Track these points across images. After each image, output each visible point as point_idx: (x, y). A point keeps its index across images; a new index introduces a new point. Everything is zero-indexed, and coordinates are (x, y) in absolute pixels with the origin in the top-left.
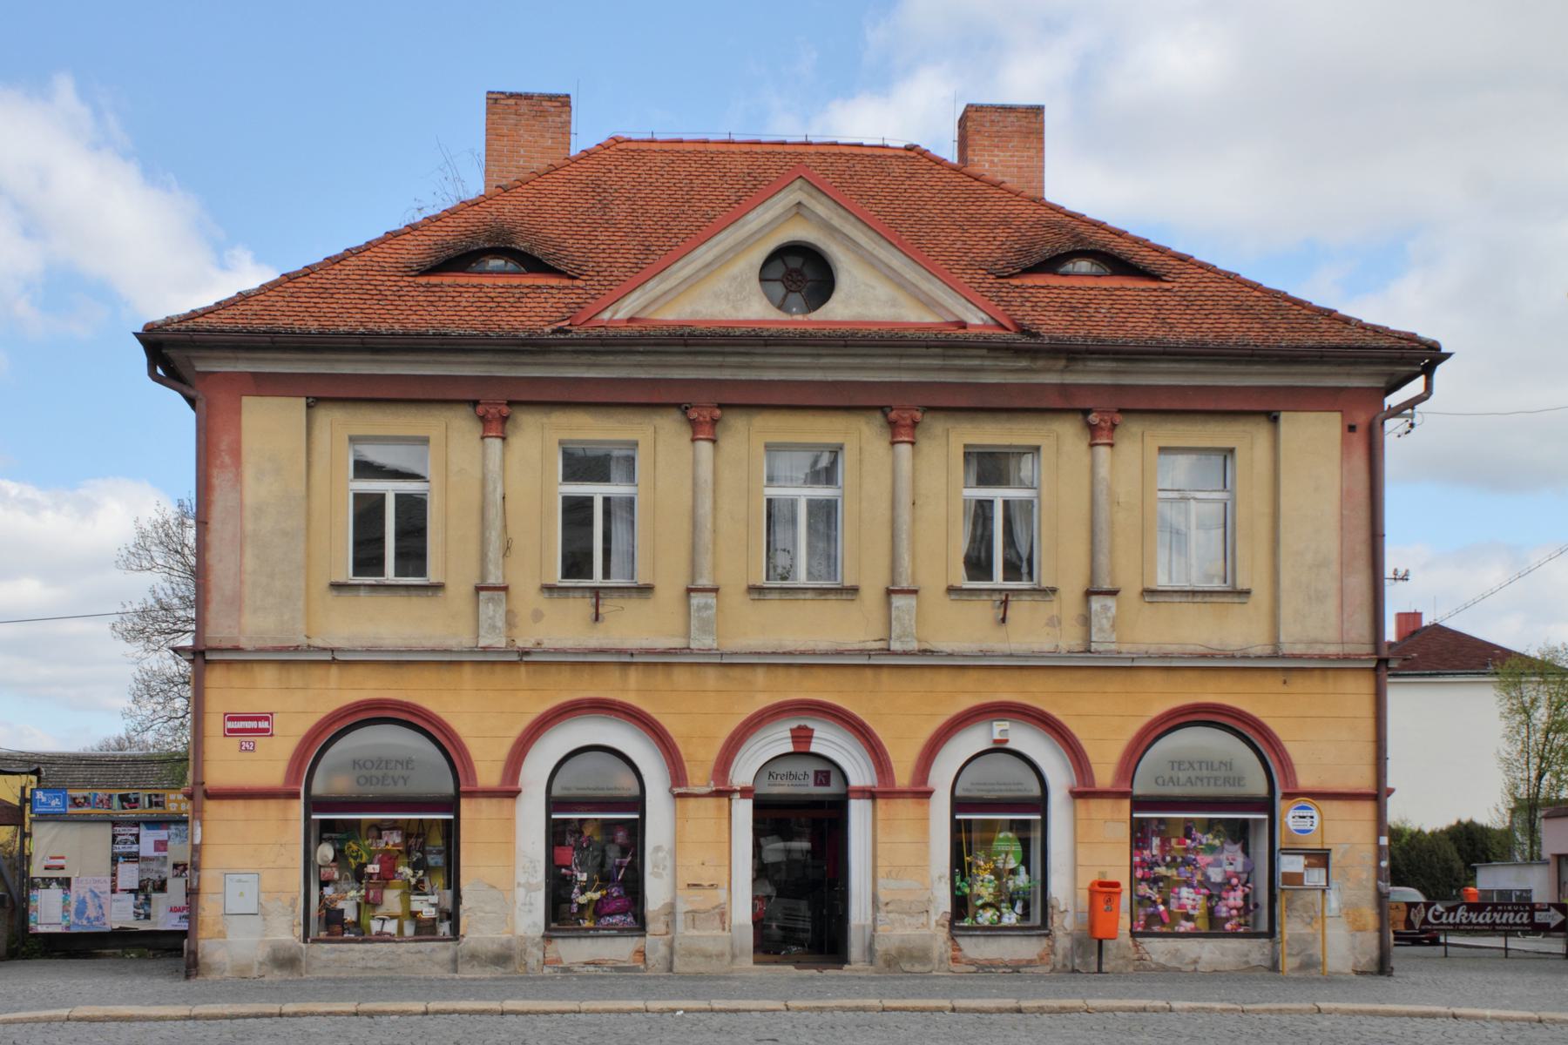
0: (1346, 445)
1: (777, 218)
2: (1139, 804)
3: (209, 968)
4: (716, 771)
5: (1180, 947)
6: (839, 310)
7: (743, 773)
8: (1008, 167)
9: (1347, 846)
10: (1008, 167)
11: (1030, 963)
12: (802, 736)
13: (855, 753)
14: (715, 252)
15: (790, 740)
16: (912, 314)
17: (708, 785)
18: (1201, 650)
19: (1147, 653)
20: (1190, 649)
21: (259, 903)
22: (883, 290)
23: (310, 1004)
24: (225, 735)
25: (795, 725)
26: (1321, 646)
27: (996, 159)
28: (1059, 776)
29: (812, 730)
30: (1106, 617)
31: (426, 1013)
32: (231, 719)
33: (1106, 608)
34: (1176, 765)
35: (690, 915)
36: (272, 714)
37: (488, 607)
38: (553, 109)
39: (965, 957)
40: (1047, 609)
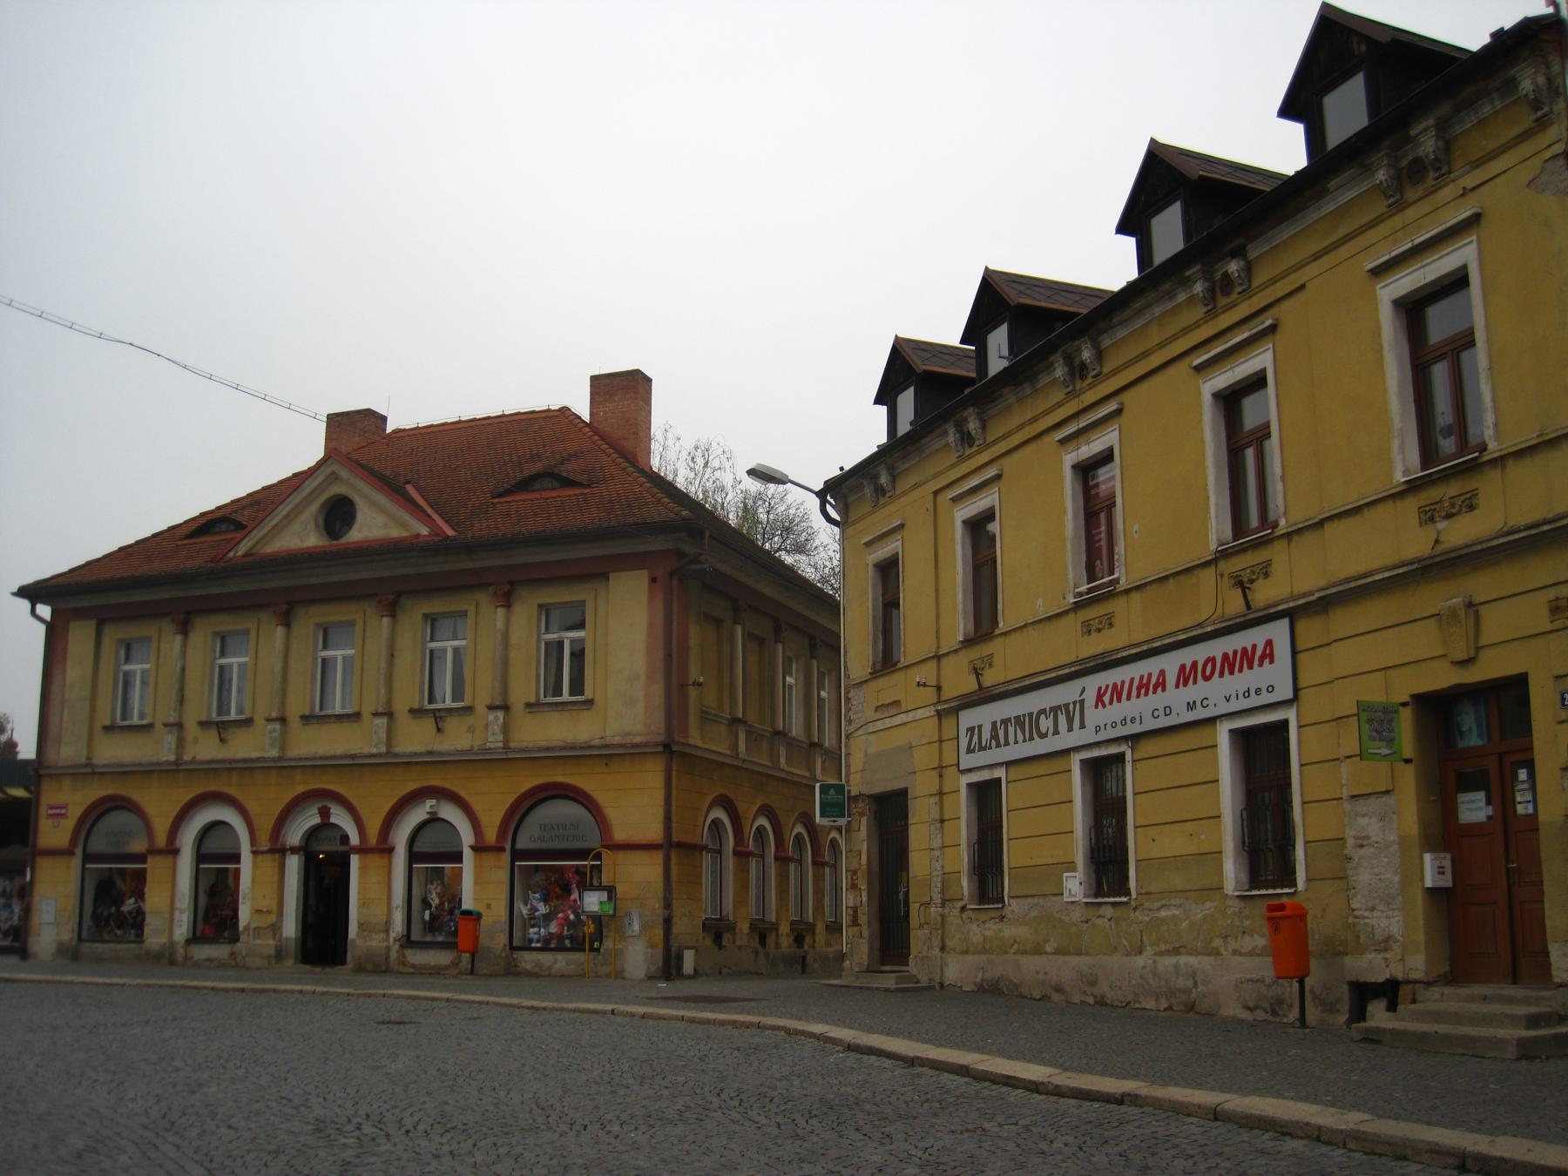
1: (321, 484)
4: (271, 837)
5: (540, 957)
7: (294, 836)
9: (645, 884)
11: (447, 967)
12: (325, 813)
14: (289, 508)
16: (396, 533)
18: (560, 744)
20: (554, 744)
22: (380, 519)
25: (320, 805)
26: (631, 737)
27: (607, 410)
28: (467, 837)
29: (330, 808)
30: (498, 725)
32: (51, 808)
33: (497, 718)
34: (543, 827)
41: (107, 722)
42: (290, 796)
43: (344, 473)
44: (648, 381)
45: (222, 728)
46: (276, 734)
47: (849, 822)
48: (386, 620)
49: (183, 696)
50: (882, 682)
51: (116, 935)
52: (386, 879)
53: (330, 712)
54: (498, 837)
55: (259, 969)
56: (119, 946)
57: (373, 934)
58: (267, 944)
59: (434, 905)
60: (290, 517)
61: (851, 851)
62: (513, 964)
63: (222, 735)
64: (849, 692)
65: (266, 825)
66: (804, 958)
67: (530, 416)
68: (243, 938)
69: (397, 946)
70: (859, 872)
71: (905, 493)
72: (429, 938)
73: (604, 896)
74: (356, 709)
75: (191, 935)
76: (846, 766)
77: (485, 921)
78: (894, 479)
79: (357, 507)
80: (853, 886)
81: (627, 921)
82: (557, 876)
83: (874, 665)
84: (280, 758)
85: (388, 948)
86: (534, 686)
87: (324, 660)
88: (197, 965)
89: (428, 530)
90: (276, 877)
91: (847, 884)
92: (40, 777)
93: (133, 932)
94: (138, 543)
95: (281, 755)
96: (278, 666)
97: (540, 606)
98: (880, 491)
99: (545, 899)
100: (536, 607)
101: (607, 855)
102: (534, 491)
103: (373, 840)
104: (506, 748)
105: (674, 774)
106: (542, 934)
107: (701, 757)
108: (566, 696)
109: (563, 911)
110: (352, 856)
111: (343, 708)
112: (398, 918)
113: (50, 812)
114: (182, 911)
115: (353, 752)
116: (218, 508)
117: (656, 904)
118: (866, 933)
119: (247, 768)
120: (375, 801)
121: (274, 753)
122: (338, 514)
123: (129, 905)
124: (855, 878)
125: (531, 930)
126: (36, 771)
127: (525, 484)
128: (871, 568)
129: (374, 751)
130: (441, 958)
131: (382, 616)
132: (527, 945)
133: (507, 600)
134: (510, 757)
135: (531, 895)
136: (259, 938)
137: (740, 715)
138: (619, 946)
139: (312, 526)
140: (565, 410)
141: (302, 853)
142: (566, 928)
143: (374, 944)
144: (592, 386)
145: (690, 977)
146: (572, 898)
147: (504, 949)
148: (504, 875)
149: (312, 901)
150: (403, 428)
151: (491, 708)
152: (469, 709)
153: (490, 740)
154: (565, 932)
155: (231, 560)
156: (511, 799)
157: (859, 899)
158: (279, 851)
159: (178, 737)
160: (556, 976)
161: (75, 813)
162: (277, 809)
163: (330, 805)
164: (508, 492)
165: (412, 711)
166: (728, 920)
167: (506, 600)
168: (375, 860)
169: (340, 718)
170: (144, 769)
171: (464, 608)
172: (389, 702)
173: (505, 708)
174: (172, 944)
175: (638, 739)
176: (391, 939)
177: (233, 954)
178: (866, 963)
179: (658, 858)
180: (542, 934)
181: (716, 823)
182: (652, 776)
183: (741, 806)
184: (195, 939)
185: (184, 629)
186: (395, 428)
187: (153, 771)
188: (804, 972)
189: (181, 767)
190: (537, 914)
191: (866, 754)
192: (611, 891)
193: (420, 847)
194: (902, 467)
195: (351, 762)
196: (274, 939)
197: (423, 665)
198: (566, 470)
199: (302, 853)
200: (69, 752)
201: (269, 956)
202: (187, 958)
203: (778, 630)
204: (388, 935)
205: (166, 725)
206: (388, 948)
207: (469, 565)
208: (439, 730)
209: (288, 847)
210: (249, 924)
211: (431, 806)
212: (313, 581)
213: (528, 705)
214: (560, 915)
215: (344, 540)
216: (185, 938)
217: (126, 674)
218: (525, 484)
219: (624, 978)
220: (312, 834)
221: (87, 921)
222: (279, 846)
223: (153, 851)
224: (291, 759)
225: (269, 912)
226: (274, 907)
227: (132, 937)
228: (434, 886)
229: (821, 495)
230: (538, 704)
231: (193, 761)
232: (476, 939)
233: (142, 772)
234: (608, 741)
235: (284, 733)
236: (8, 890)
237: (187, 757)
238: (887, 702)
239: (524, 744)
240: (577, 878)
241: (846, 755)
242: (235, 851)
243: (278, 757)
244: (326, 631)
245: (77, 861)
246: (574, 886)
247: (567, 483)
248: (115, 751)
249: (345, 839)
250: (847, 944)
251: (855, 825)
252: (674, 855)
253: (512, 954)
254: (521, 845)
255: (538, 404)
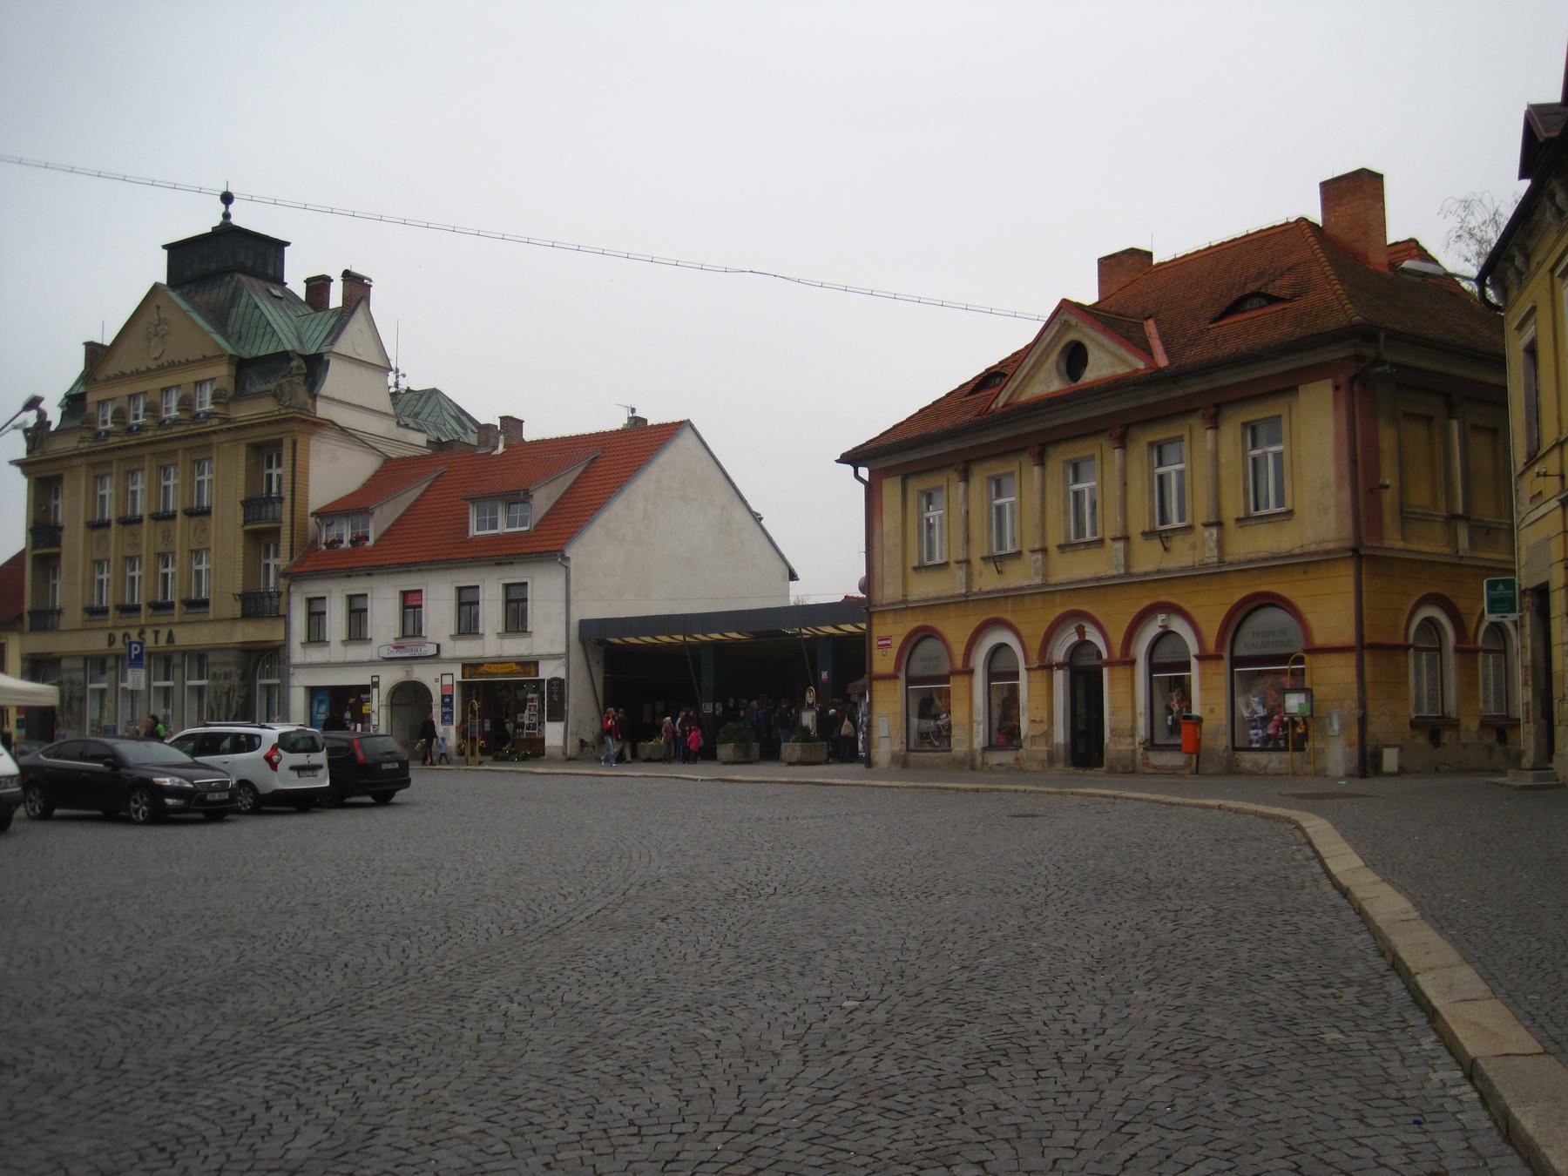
0: (1335, 398)
1: (1058, 331)
7: (1059, 653)
11: (1181, 768)
12: (1081, 631)
13: (1062, 639)
14: (1034, 359)
16: (1121, 370)
18: (1267, 555)
20: (1261, 555)
22: (1107, 359)
25: (1077, 624)
28: (1193, 648)
31: (1025, 791)
33: (1211, 534)
42: (1052, 618)
43: (1073, 320)
45: (997, 561)
46: (1039, 564)
48: (1117, 452)
55: (1035, 771)
56: (936, 754)
58: (1040, 750)
65: (1035, 644)
68: (1025, 745)
72: (1171, 742)
75: (987, 745)
85: (1134, 752)
87: (1255, 460)
88: (991, 770)
90: (1045, 692)
92: (870, 615)
96: (1037, 502)
97: (1244, 425)
100: (1239, 427)
102: (1245, 312)
103: (1117, 654)
104: (1221, 562)
105: (1364, 577)
107: (1400, 558)
112: (1142, 723)
113: (880, 643)
117: (1352, 704)
120: (1117, 617)
121: (1038, 580)
122: (1075, 358)
125: (1252, 732)
127: (1236, 307)
128: (1521, 354)
129: (1115, 572)
130: (1174, 759)
133: (1214, 423)
137: (1460, 510)
139: (1054, 373)
151: (1207, 525)
154: (1281, 733)
155: (994, 411)
156: (1225, 610)
158: (1048, 667)
161: (896, 643)
162: (1042, 631)
163: (1084, 624)
164: (1223, 316)
168: (1121, 672)
169: (1088, 544)
171: (1276, 413)
172: (1125, 527)
174: (972, 752)
175: (1331, 546)
176: (1137, 743)
177: (1017, 759)
181: (1430, 622)
182: (1343, 580)
184: (990, 747)
200: (889, 592)
201: (1043, 760)
202: (984, 763)
204: (1134, 740)
205: (957, 562)
206: (1134, 752)
207: (1179, 393)
208: (1166, 549)
212: (1058, 422)
215: (1080, 382)
218: (1236, 307)
219: (1325, 776)
220: (1075, 650)
222: (1046, 662)
224: (1056, 585)
225: (1042, 722)
231: (980, 592)
232: (1198, 742)
234: (1306, 549)
235: (1045, 562)
237: (975, 589)
245: (902, 683)
247: (1272, 300)
248: (925, 588)
249: (1099, 652)
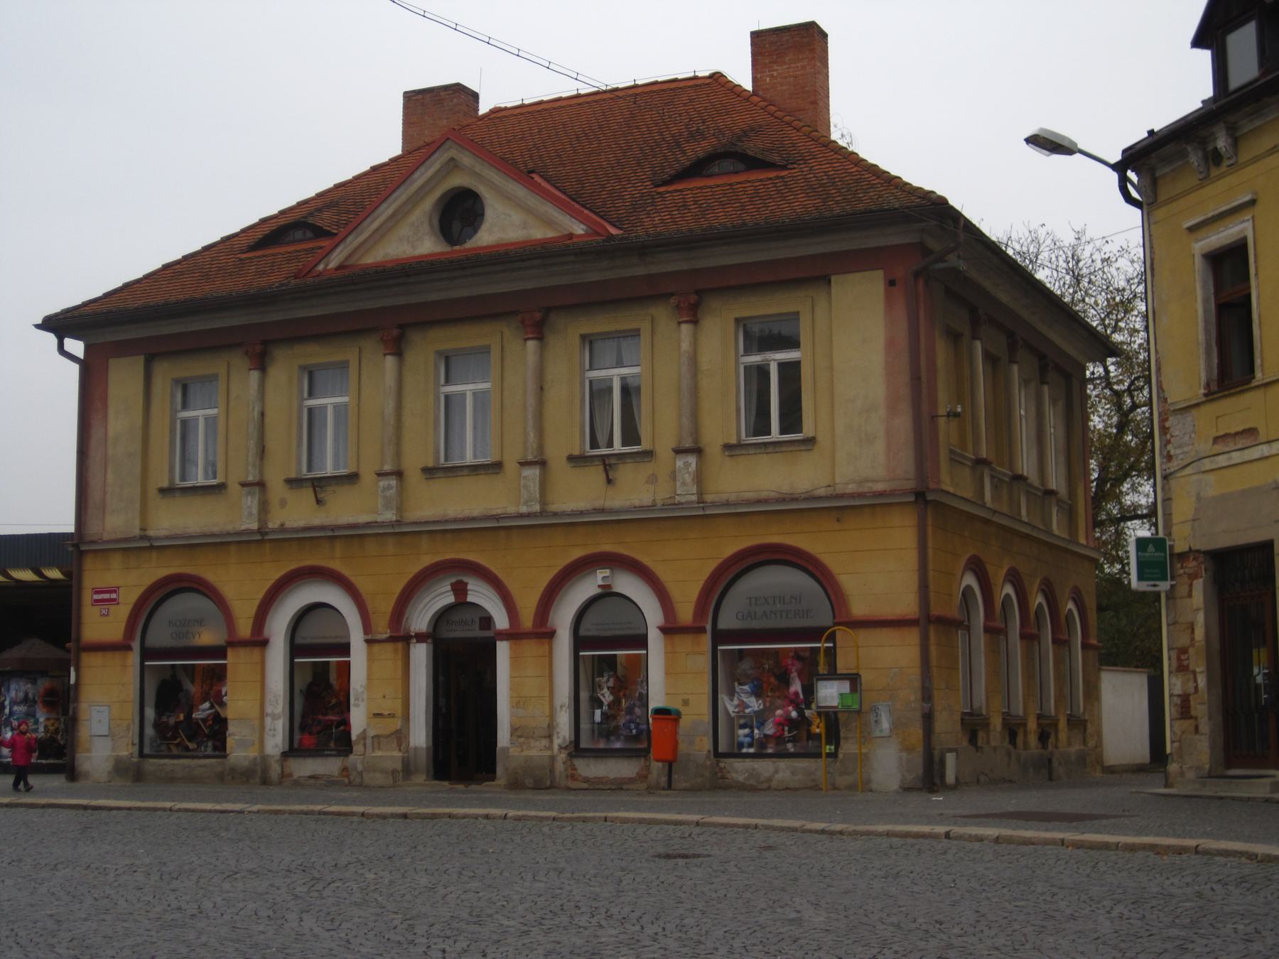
2: (720, 637)
3: (86, 775)
5: (756, 766)
6: (487, 236)
7: (420, 619)
8: (786, 78)
10: (786, 78)
11: (631, 781)
12: (460, 589)
15: (452, 593)
16: (539, 233)
17: (386, 633)
19: (728, 501)
20: (764, 495)
21: (110, 728)
22: (516, 217)
23: (968, 828)
24: (92, 605)
25: (454, 580)
26: (870, 484)
27: (775, 74)
28: (653, 615)
29: (466, 584)
30: (688, 473)
33: (687, 465)
35: (376, 740)
36: (118, 588)
37: (247, 499)
38: (447, 97)
39: (580, 776)
40: (647, 468)
41: (165, 484)
43: (466, 159)
44: (824, 36)
46: (393, 492)
47: (1172, 586)
48: (531, 345)
49: (264, 447)
50: (1225, 405)
51: (187, 749)
52: (547, 671)
53: (458, 462)
54: (125, 635)
57: (532, 741)
58: (391, 756)
59: (606, 703)
60: (397, 218)
61: (1175, 623)
62: (719, 774)
63: (319, 496)
64: (1167, 419)
65: (383, 607)
66: (1050, 761)
67: (673, 85)
68: (358, 748)
69: (563, 756)
70: (1191, 651)
71: (1256, 160)
72: (602, 745)
73: (845, 687)
74: (352, 469)
75: (287, 748)
76: (1164, 514)
77: (684, 722)
78: (1236, 142)
79: (485, 202)
80: (1182, 668)
81: (872, 718)
82: (771, 662)
83: (1208, 385)
84: (399, 523)
85: (553, 759)
86: (734, 425)
88: (297, 783)
89: (584, 227)
91: (1170, 665)
93: (210, 744)
94: (185, 258)
95: (399, 519)
98: (1215, 158)
99: (757, 693)
101: (842, 635)
103: (527, 621)
106: (757, 736)
108: (775, 434)
109: (783, 707)
110: (498, 643)
111: (475, 456)
112: (564, 720)
113: (96, 597)
114: (275, 718)
115: (494, 512)
116: (282, 213)
117: (910, 695)
118: (1205, 727)
119: (353, 536)
121: (390, 516)
123: (203, 711)
124: (1183, 657)
126: (76, 546)
127: (697, 169)
128: (1198, 261)
131: (526, 340)
132: (736, 751)
134: (336, 534)
135: (738, 688)
136: (379, 749)
138: (864, 751)
139: (426, 227)
140: (717, 78)
141: (430, 641)
142: (786, 728)
143: (534, 753)
144: (753, 44)
145: (954, 788)
146: (792, 689)
147: (708, 757)
148: (704, 662)
149: (442, 702)
150: (503, 106)
151: (679, 451)
152: (649, 454)
153: (679, 492)
154: (786, 734)
155: (320, 274)
156: (711, 566)
157: (1191, 685)
158: (402, 639)
159: (259, 499)
160: (776, 789)
161: (129, 598)
165: (571, 458)
166: (981, 715)
167: (692, 313)
168: (531, 648)
169: (475, 469)
170: (218, 540)
173: (698, 451)
175: (880, 487)
176: (556, 747)
177: (345, 769)
178: (1208, 766)
179: (912, 637)
180: (757, 736)
183: (991, 569)
184: (293, 751)
185: (261, 363)
186: (491, 107)
187: (228, 543)
188: (1050, 779)
189: (266, 538)
190: (747, 711)
191: (1199, 498)
192: (854, 679)
193: (587, 630)
194: (1250, 127)
195: (496, 525)
196: (400, 750)
197: (300, 438)
198: (753, 147)
199: (430, 641)
201: (394, 772)
202: (284, 775)
203: (1012, 347)
204: (551, 742)
205: (244, 485)
206: (553, 759)
207: (640, 271)
208: (609, 481)
209: (413, 634)
210: (365, 731)
211: (604, 578)
212: (433, 297)
213: (727, 447)
214: (779, 712)
215: (470, 244)
216: (281, 751)
217: (185, 423)
218: (697, 169)
219: (871, 791)
220: (442, 617)
221: (150, 731)
223: (235, 643)
225: (392, 716)
226: (399, 711)
227: (209, 751)
228: (605, 679)
229: (1120, 168)
230: (739, 446)
231: (282, 528)
233: (216, 544)
234: (840, 489)
235: (401, 490)
236: (30, 696)
238: (1233, 431)
239: (724, 497)
240: (798, 665)
241: (1164, 501)
242: (343, 641)
243: (396, 521)
244: (447, 360)
245: (134, 658)
246: (794, 674)
247: (754, 163)
249: (487, 621)
250: (1172, 742)
251: (1182, 590)
252: (932, 629)
253: (718, 763)
254: (722, 625)
255: (682, 71)
